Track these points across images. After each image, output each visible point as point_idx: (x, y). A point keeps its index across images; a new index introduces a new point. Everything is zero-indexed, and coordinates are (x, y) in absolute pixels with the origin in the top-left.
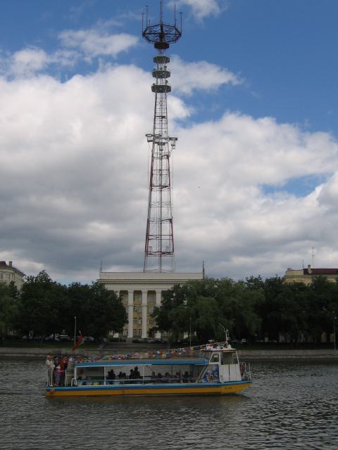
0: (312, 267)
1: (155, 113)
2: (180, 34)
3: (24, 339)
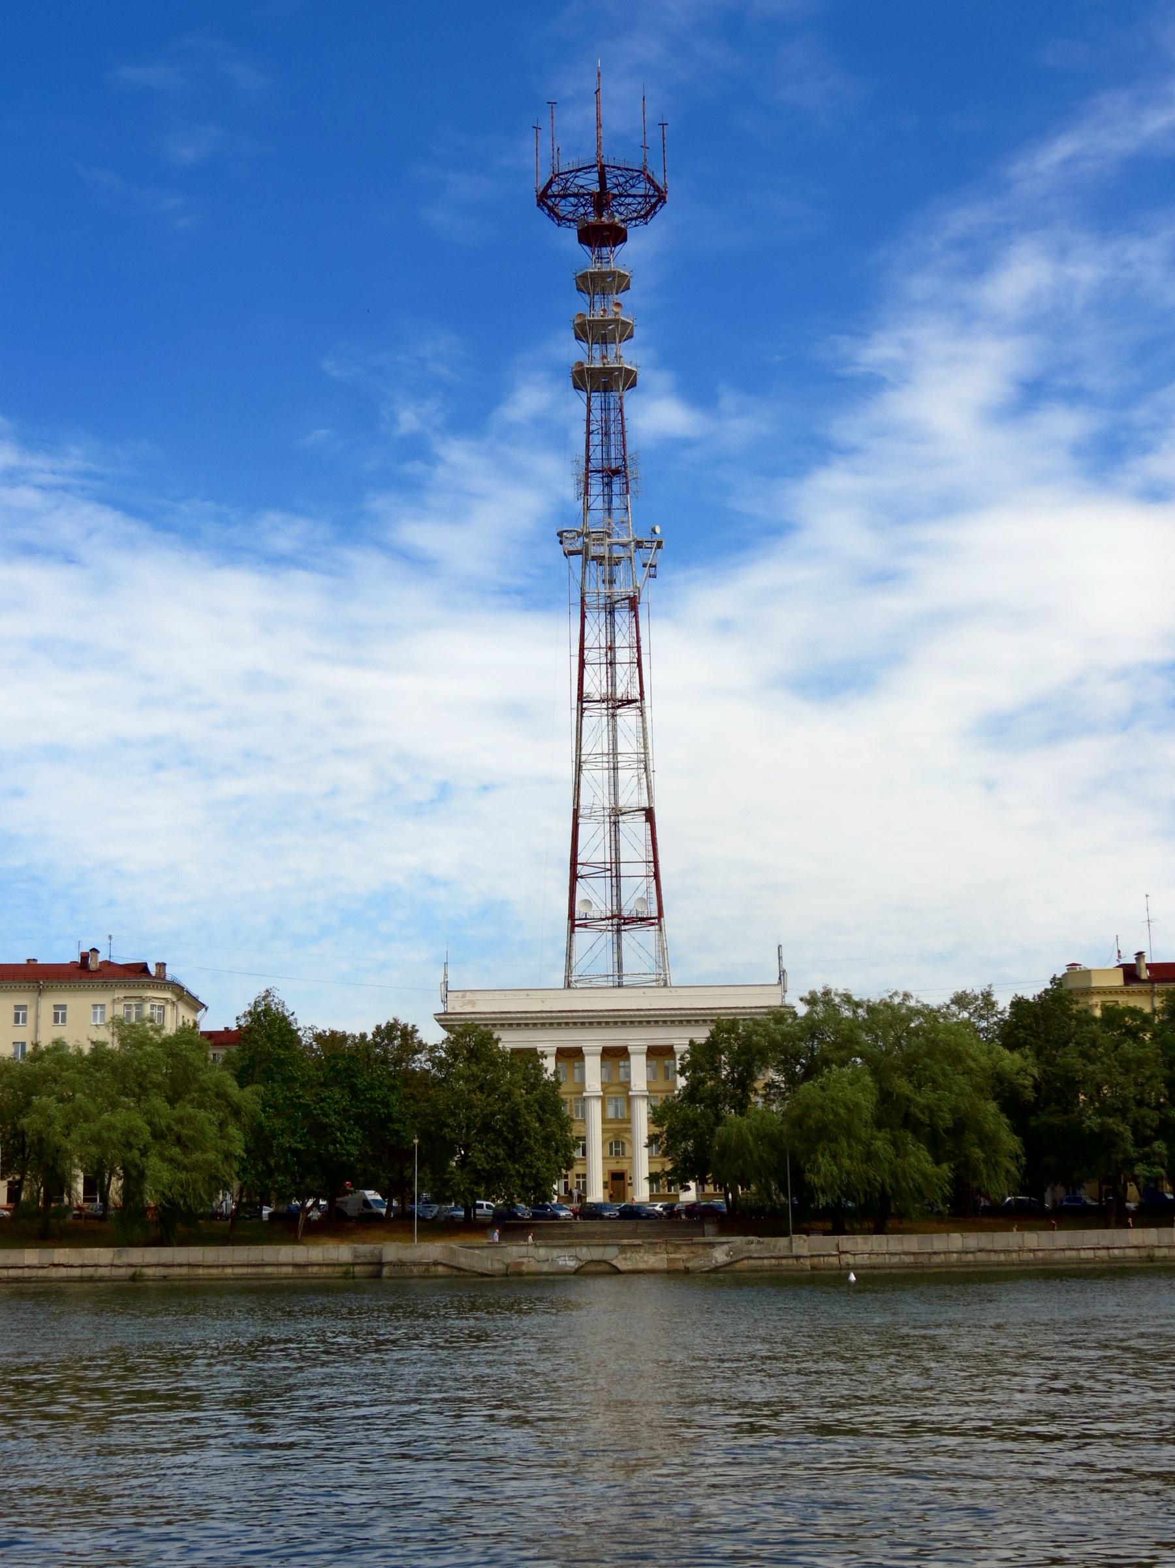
0: (1147, 960)
1: (588, 460)
2: (662, 199)
3: (324, 1199)
